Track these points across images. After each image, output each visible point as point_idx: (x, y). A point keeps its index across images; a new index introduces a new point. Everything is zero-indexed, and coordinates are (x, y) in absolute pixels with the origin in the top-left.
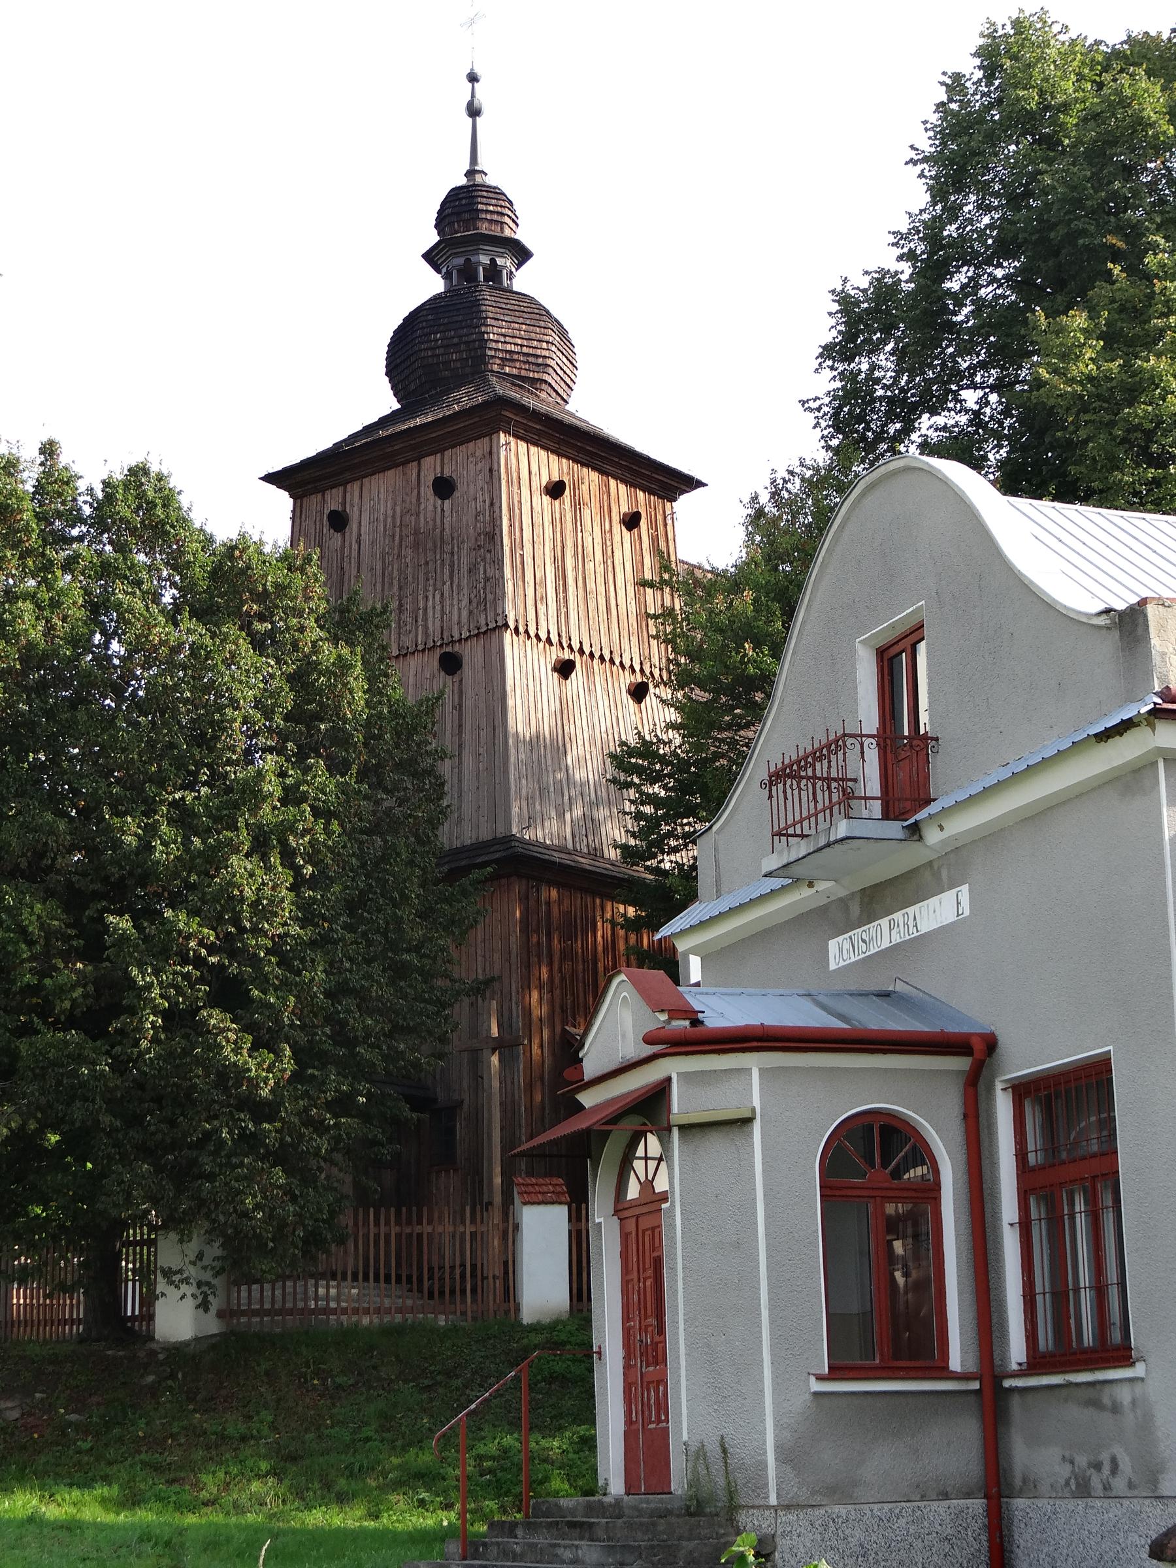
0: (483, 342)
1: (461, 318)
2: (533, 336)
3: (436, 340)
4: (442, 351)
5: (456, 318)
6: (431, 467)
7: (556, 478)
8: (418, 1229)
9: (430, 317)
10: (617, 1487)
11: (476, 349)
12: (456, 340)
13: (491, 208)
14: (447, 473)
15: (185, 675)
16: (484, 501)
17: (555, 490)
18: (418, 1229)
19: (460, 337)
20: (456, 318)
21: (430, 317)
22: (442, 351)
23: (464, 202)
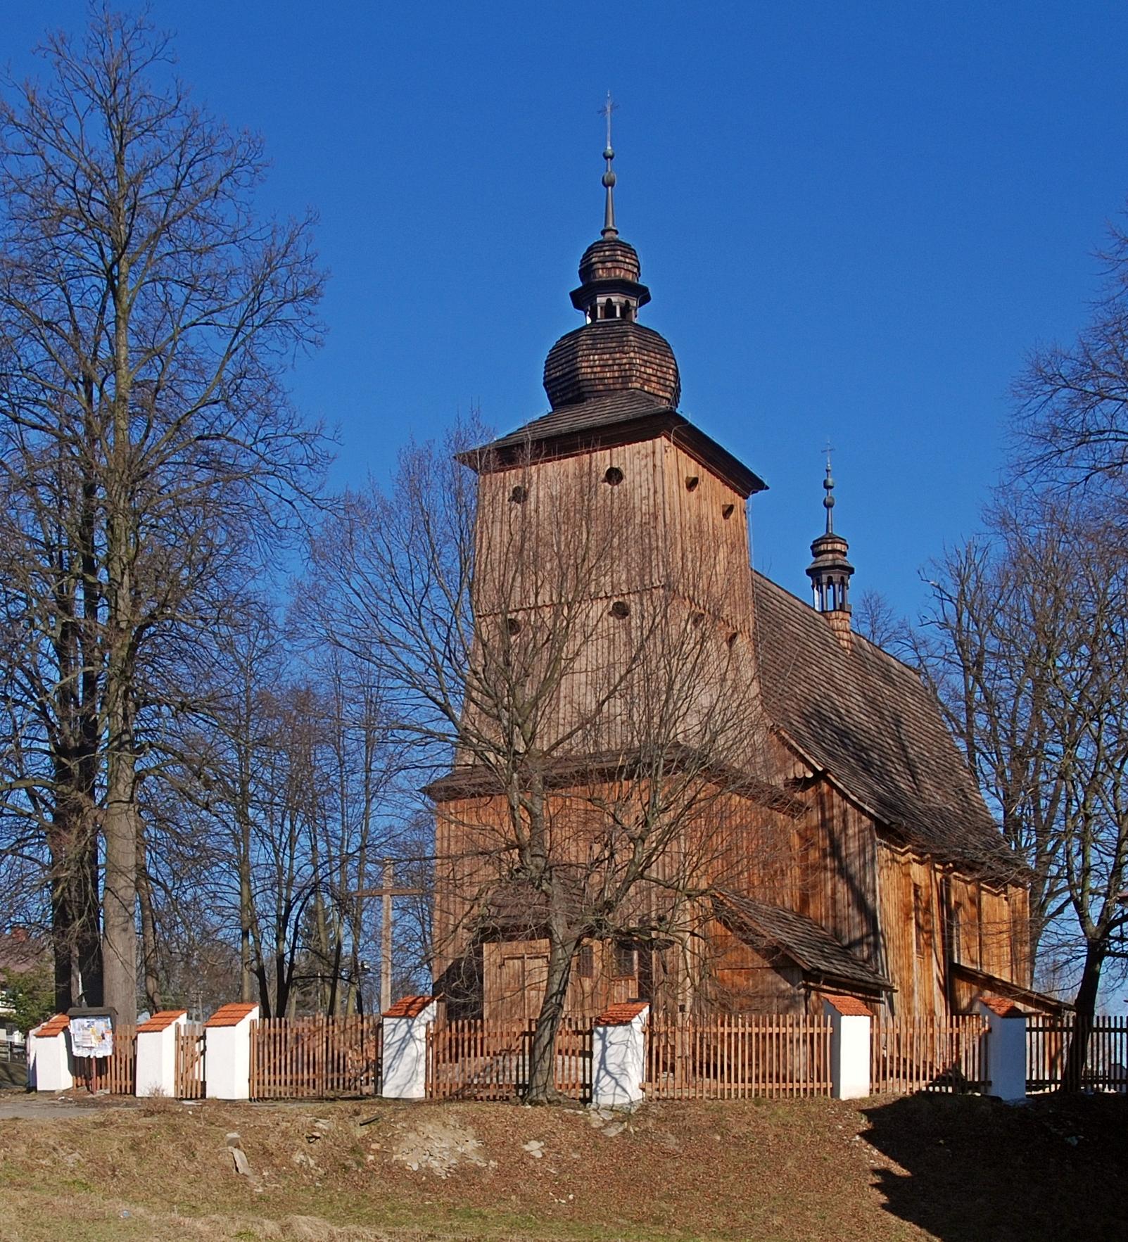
0: (963, 980)
1: (614, 345)
2: (664, 363)
3: (594, 361)
4: (599, 369)
5: (610, 345)
6: (603, 459)
7: (693, 475)
8: (769, 1030)
9: (589, 342)
10: (905, 1172)
11: (626, 370)
12: (610, 362)
13: (627, 260)
14: (615, 465)
15: (601, 819)
16: (649, 489)
17: (692, 484)
18: (769, 1030)
19: (614, 360)
20: (610, 345)
21: (589, 342)
22: (599, 369)
23: (607, 253)
